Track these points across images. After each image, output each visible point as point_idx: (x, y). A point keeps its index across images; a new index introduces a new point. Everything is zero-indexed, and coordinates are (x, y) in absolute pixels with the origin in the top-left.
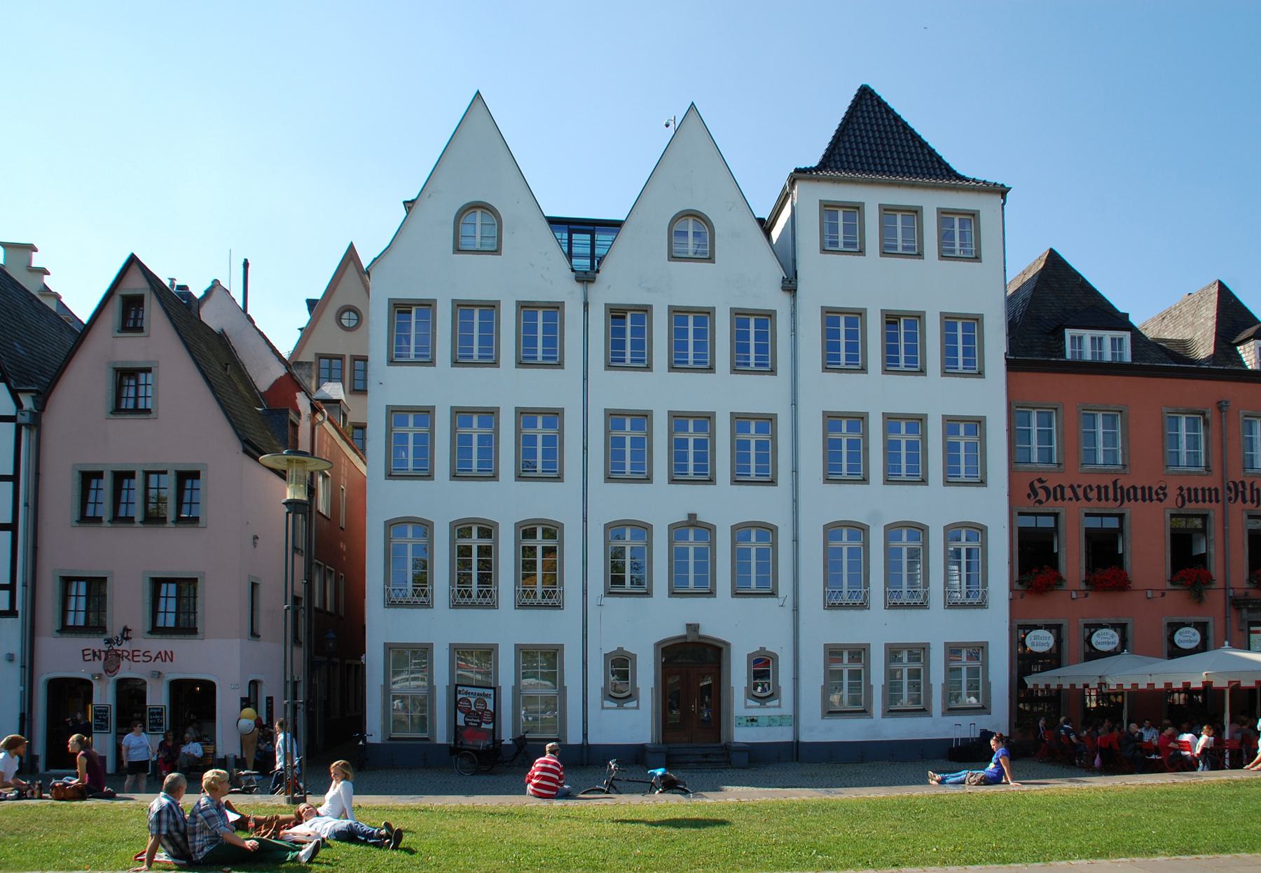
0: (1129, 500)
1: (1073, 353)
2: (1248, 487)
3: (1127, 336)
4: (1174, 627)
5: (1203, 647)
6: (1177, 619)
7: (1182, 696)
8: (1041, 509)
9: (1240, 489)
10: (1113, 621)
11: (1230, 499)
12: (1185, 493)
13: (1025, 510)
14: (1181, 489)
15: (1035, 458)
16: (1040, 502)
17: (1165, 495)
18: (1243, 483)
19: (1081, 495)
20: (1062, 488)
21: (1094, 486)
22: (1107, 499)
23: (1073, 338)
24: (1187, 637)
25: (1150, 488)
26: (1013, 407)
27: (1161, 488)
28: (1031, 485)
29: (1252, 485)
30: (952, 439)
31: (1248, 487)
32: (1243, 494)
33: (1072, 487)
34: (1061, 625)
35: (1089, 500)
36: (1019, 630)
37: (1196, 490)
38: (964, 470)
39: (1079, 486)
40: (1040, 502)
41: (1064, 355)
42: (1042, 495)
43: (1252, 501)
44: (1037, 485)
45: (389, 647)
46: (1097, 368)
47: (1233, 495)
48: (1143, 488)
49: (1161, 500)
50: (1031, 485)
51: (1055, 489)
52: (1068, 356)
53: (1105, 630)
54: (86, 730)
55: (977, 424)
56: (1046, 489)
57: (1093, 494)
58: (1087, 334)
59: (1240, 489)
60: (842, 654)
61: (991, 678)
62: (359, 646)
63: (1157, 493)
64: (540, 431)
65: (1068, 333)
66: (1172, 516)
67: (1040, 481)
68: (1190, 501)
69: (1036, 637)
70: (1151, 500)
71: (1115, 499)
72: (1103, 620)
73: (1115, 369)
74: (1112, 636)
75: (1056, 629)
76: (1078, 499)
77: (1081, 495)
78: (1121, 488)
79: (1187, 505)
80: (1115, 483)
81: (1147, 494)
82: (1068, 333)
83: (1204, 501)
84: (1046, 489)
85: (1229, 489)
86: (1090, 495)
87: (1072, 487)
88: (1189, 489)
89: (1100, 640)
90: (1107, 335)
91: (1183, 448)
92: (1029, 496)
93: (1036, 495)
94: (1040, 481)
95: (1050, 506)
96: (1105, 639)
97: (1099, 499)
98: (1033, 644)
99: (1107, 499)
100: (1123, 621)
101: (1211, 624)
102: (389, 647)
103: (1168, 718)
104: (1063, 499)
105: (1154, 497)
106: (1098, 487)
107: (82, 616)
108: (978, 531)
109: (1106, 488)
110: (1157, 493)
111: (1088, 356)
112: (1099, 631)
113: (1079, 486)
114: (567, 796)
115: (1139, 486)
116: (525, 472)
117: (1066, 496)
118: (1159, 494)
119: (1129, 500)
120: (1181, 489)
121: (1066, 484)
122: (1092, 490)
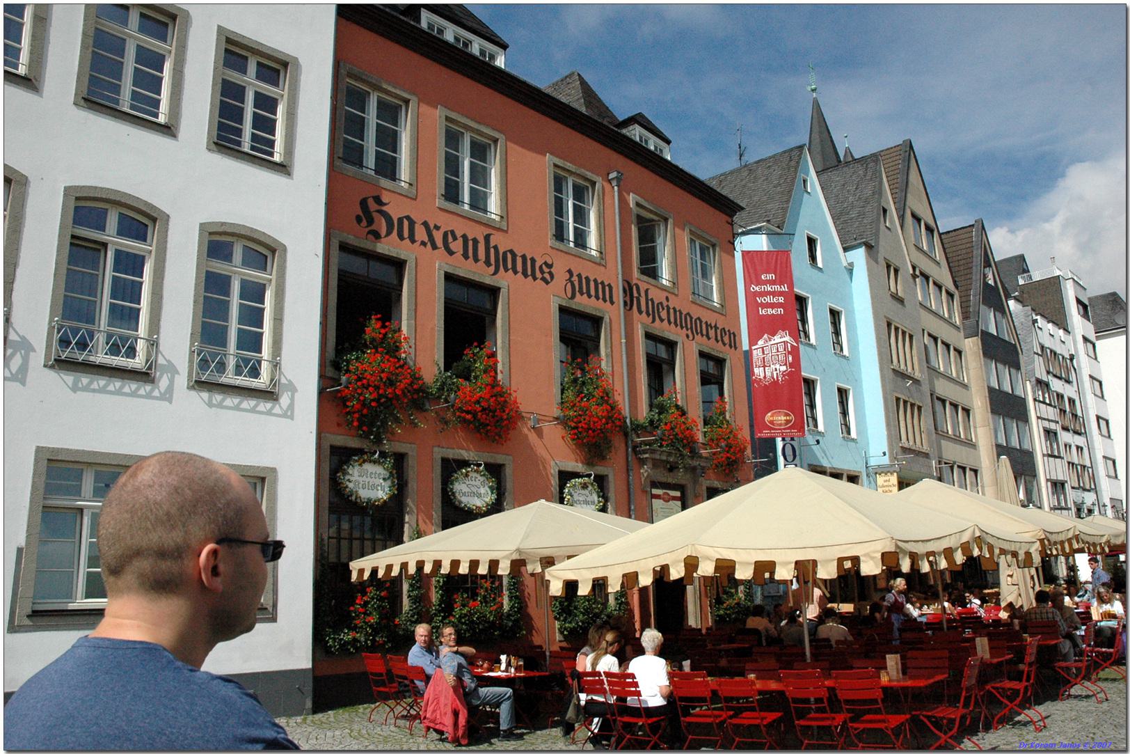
0: (506, 270)
5: (496, 507)
19: (439, 242)
21: (459, 234)
24: (473, 490)
25: (533, 260)
26: (343, 71)
28: (363, 203)
31: (643, 294)
33: (425, 224)
34: (561, 473)
35: (451, 253)
36: (334, 462)
43: (488, 263)
50: (363, 203)
57: (457, 246)
60: (79, 478)
64: (251, 83)
75: (398, 465)
76: (434, 247)
77: (439, 242)
78: (496, 248)
81: (531, 269)
86: (453, 246)
92: (359, 219)
93: (371, 221)
101: (611, 478)
105: (538, 275)
106: (464, 237)
108: (264, 252)
109: (475, 241)
114: (520, 737)
118: (544, 273)
120: (570, 271)
121: (418, 218)
122: (455, 238)
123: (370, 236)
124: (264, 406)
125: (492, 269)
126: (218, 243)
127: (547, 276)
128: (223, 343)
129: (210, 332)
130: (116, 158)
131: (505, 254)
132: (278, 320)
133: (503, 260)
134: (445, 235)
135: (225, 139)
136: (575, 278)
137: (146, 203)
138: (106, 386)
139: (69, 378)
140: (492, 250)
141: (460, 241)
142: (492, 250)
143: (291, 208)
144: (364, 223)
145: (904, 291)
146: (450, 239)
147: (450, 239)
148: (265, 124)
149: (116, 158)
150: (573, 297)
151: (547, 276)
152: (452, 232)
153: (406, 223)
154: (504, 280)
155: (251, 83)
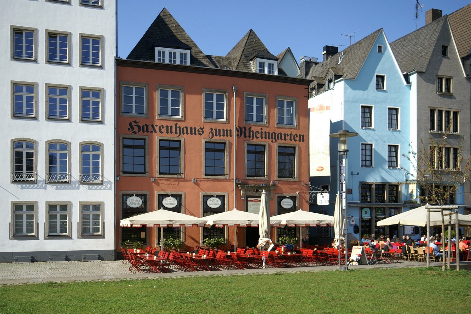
0: (184, 134)
1: (159, 60)
2: (247, 130)
3: (188, 52)
4: (206, 197)
6: (209, 193)
8: (135, 136)
9: (243, 130)
10: (174, 193)
12: (214, 131)
13: (127, 136)
14: (212, 129)
15: (134, 111)
16: (135, 133)
17: (203, 132)
18: (245, 128)
20: (147, 126)
21: (164, 126)
22: (171, 133)
24: (287, 203)
25: (195, 128)
27: (201, 128)
28: (130, 124)
29: (250, 129)
30: (19, 94)
31: (247, 130)
32: (245, 133)
35: (162, 133)
36: (121, 198)
37: (220, 130)
38: (90, 114)
39: (156, 126)
40: (135, 133)
41: (154, 60)
42: (136, 129)
44: (133, 124)
45: (258, 214)
46: (172, 68)
48: (191, 128)
49: (201, 135)
50: (130, 124)
51: (143, 127)
52: (156, 61)
53: (214, 198)
54: (160, 260)
55: (97, 93)
56: (139, 127)
57: (164, 130)
58: (167, 51)
59: (243, 130)
61: (105, 221)
63: (198, 130)
65: (157, 49)
66: (206, 142)
67: (135, 122)
68: (216, 135)
69: (132, 200)
70: (195, 134)
71: (176, 133)
72: (169, 193)
73: (182, 68)
74: (290, 202)
78: (179, 127)
79: (215, 137)
81: (193, 131)
82: (157, 49)
83: (224, 135)
88: (216, 130)
89: (167, 202)
90: (178, 52)
91: (255, 113)
92: (129, 129)
93: (133, 129)
94: (135, 122)
95: (141, 135)
96: (287, 203)
97: (167, 132)
98: (131, 203)
99: (171, 133)
100: (179, 193)
102: (258, 214)
104: (148, 131)
105: (197, 132)
108: (97, 147)
110: (198, 130)
111: (167, 61)
112: (167, 198)
113: (156, 126)
115: (189, 127)
116: (51, 116)
117: (149, 130)
119: (184, 134)
120: (212, 129)
123: (133, 134)
124: (66, 186)
125: (178, 135)
126: (85, 92)
127: (201, 133)
128: (89, 171)
129: (85, 169)
130: (24, 72)
131: (183, 129)
132: (103, 164)
133: (182, 131)
134: (160, 127)
135: (84, 62)
136: (214, 131)
137: (65, 141)
138: (29, 186)
139: (19, 186)
140: (178, 129)
141: (165, 128)
142: (178, 129)
143: (104, 134)
144: (131, 130)
145: (454, 89)
146: (162, 128)
147: (162, 128)
148: (96, 110)
149: (24, 72)
150: (213, 137)
151: (201, 133)
152: (162, 126)
153: (145, 127)
154: (182, 137)
155: (91, 100)
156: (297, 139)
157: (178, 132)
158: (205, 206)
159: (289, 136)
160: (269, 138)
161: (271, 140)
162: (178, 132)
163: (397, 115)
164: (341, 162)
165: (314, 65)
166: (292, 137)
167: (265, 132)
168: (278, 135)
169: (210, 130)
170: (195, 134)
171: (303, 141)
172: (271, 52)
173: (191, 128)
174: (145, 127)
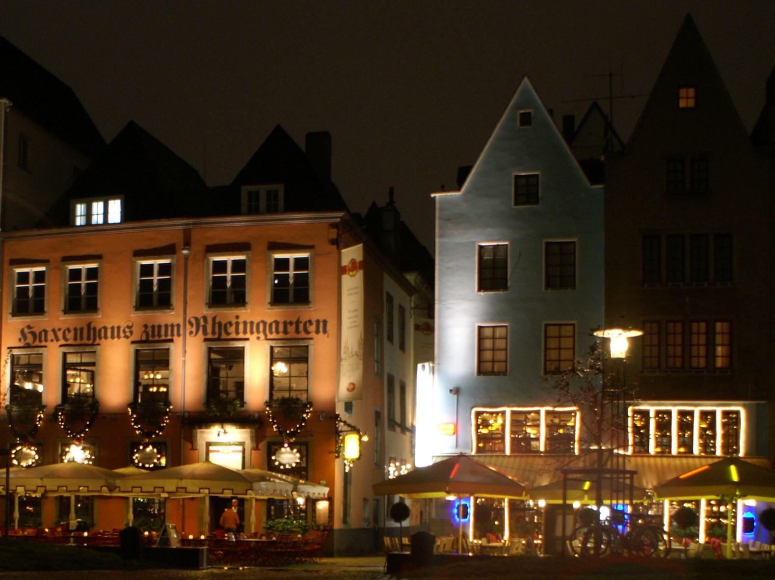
7: (572, 433)
9: (202, 323)
11: (191, 333)
12: (150, 330)
14: (146, 326)
17: (131, 333)
20: (46, 332)
21: (313, 320)
23: (250, 194)
32: (205, 328)
44: (26, 331)
47: (194, 329)
51: (40, 333)
56: (33, 334)
59: (202, 323)
62: (519, 84)
63: (124, 332)
80: (89, 325)
84: (33, 334)
85: (191, 324)
87: (54, 330)
103: (542, 513)
105: (122, 334)
107: (695, 329)
113: (59, 330)
134: (305, 324)
141: (315, 324)
144: (23, 341)
151: (128, 334)
156: (312, 328)
157: (92, 336)
158: (638, 444)
159: (294, 326)
160: (252, 333)
161: (255, 335)
162: (92, 336)
163: (575, 246)
164: (378, 369)
165: (82, 214)
166: (301, 326)
167: (245, 323)
168: (100, 330)
169: (144, 329)
170: (119, 337)
171: (325, 331)
172: (334, 179)
173: (113, 328)
174: (43, 333)
